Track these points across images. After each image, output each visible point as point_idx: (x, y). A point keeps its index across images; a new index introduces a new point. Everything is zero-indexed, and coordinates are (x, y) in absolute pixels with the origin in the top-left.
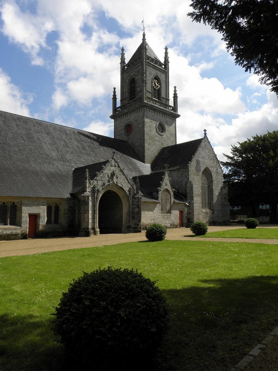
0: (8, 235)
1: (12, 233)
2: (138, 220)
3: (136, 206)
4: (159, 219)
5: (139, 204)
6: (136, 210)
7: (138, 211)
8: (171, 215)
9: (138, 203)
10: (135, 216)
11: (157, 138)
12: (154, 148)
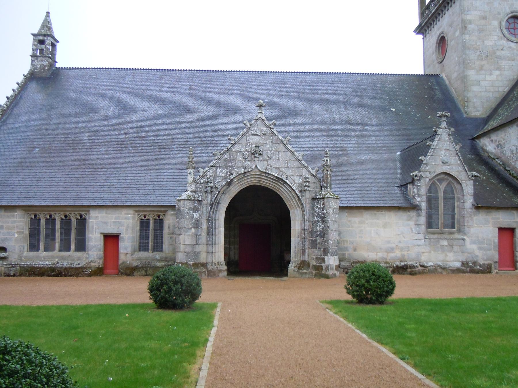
0: (66, 268)
1: (72, 266)
2: (322, 250)
3: (319, 219)
4: (417, 249)
5: (324, 214)
6: (318, 228)
7: (323, 228)
8: (464, 240)
9: (323, 210)
10: (316, 241)
11: (503, 53)
12: (495, 77)
